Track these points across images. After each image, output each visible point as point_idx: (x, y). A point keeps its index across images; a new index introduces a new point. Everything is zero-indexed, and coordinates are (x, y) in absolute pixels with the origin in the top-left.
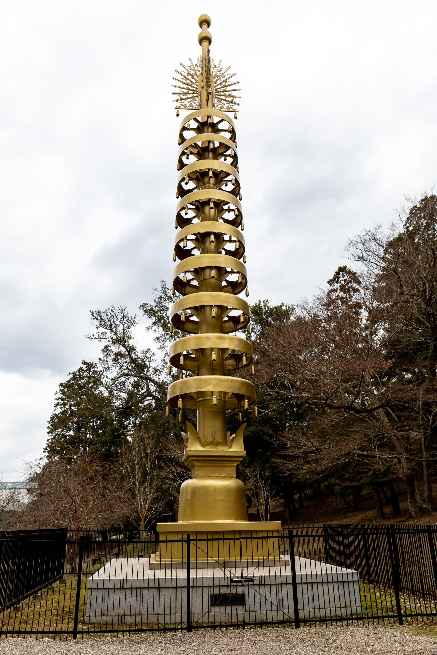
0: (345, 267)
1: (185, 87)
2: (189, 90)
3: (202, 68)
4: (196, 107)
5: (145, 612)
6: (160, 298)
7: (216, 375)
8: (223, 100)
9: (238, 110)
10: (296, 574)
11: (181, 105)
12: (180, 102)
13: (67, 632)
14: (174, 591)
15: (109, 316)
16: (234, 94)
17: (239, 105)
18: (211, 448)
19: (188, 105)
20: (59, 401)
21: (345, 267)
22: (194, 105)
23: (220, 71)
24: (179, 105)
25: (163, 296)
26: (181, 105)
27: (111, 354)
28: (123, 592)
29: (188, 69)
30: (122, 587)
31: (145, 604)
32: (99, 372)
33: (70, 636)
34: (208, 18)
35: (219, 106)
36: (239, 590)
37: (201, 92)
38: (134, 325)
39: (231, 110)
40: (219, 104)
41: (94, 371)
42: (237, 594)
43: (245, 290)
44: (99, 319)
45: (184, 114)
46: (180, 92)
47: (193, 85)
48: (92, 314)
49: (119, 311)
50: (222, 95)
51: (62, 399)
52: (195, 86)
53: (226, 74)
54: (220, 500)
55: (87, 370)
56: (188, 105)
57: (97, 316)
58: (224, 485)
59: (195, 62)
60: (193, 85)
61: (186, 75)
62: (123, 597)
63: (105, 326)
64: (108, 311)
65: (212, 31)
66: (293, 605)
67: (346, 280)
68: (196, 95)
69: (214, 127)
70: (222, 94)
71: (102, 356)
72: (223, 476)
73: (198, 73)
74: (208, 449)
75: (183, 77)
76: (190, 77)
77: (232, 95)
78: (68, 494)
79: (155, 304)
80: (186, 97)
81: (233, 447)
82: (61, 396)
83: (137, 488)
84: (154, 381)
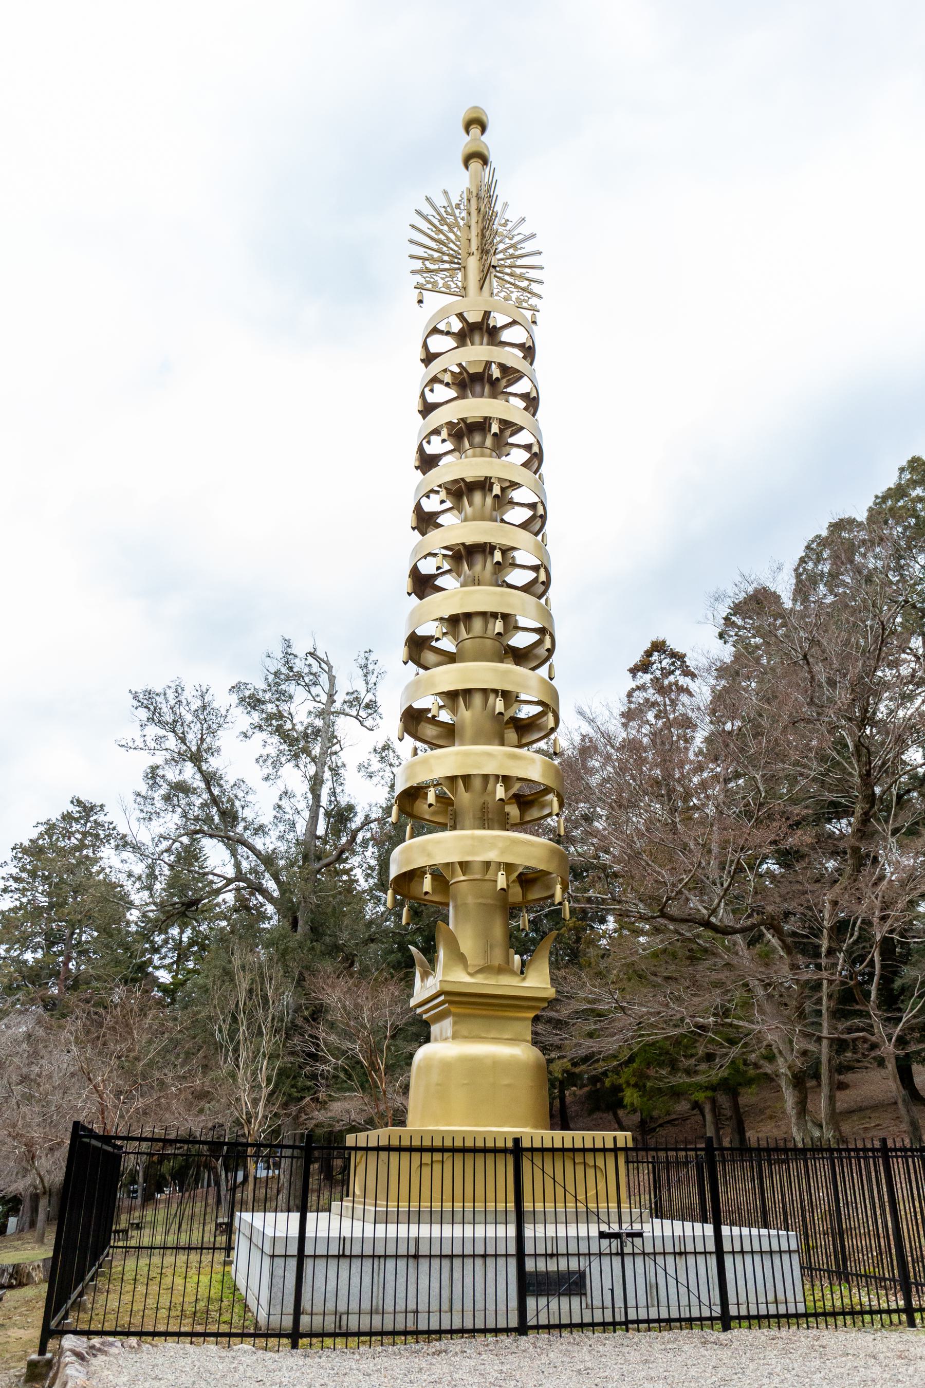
0: (664, 642)
1: (436, 247)
2: (443, 253)
3: (469, 214)
5: (389, 1307)
6: (277, 674)
7: (493, 829)
8: (510, 283)
9: (539, 307)
11: (428, 282)
12: (425, 275)
14: (446, 1263)
15: (172, 702)
16: (532, 274)
17: (540, 297)
18: (486, 979)
19: (441, 285)
20: (8, 884)
21: (664, 642)
22: (453, 286)
23: (505, 225)
24: (422, 281)
25: (284, 670)
26: (428, 282)
27: (161, 783)
28: (344, 1263)
29: (442, 210)
30: (341, 1253)
32: (106, 825)
34: (484, 118)
35: (503, 294)
38: (225, 726)
39: (525, 305)
40: (502, 291)
41: (95, 821)
42: (570, 1273)
43: (548, 664)
44: (152, 708)
46: (426, 255)
47: (452, 245)
48: (135, 697)
49: (195, 693)
50: (507, 274)
51: (17, 879)
52: (456, 248)
53: (515, 233)
54: (506, 1085)
55: (81, 818)
56: (441, 285)
57: (147, 701)
58: (512, 1056)
59: (455, 201)
60: (452, 245)
61: (437, 224)
62: (344, 1274)
63: (162, 723)
64: (168, 691)
65: (491, 141)
67: (665, 668)
68: (456, 266)
69: (492, 334)
70: (508, 270)
71: (143, 789)
72: (506, 1037)
73: (462, 223)
74: (480, 979)
76: (445, 228)
77: (527, 275)
78: (89, 1079)
79: (264, 686)
80: (436, 267)
81: (528, 980)
82: (15, 871)
83: (242, 1072)
84: (255, 849)
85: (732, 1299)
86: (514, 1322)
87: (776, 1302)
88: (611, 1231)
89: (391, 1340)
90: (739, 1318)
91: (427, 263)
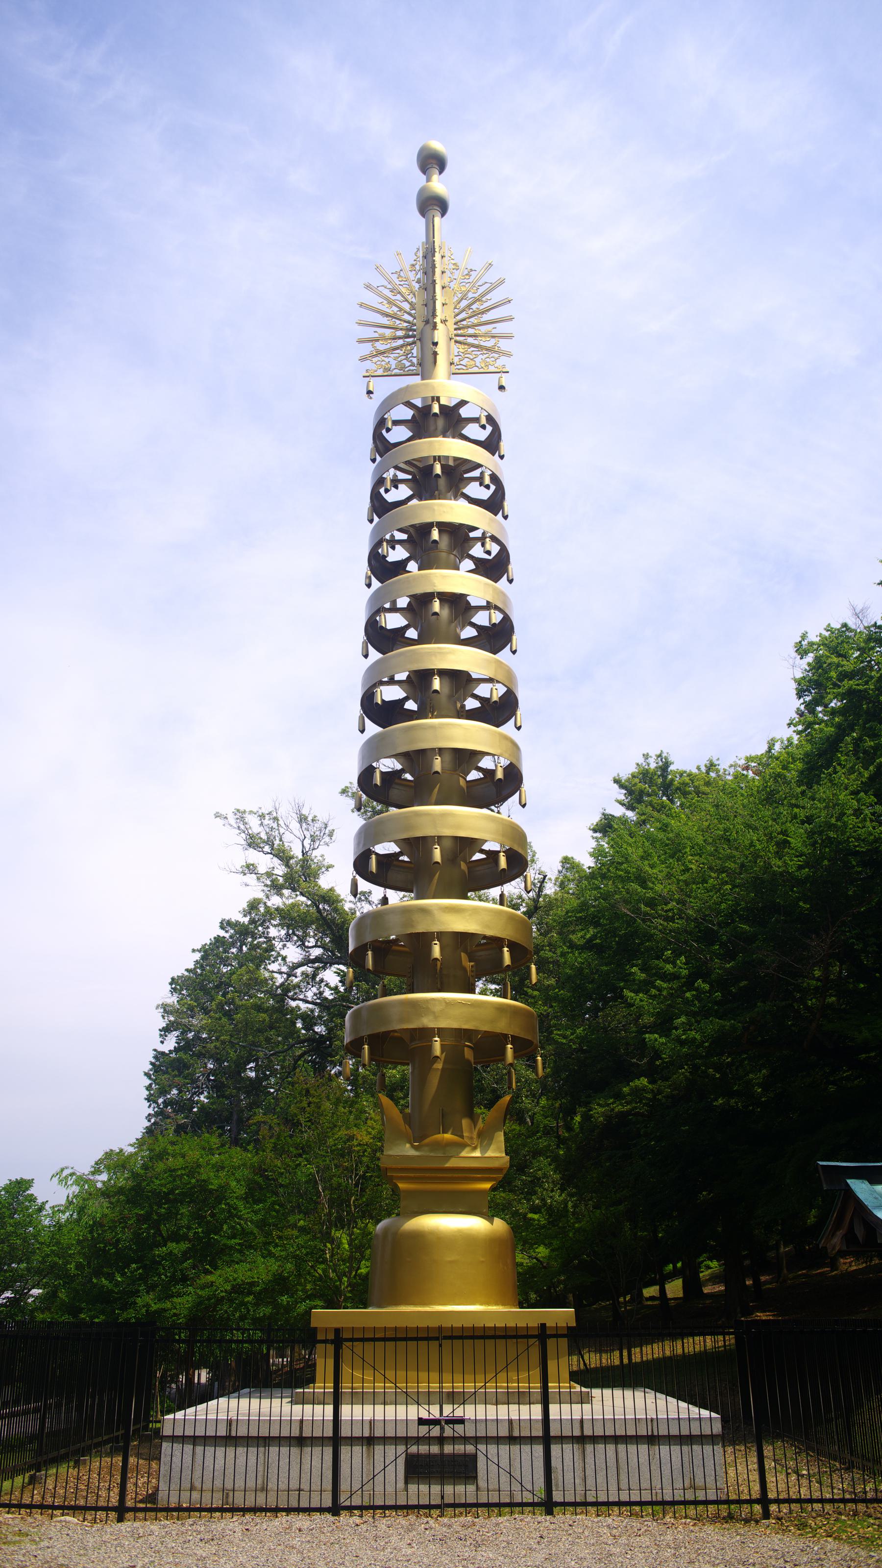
4: (412, 368)
10: (551, 1417)
13: (106, 1509)
16: (500, 328)
31: (273, 1471)
33: (113, 1515)
36: (470, 1449)
37: (422, 333)
42: (465, 1455)
45: (385, 388)
52: (411, 319)
66: (542, 1480)
68: (411, 340)
75: (381, 300)
77: (494, 331)
85: (344, 1486)
86: (328, 1502)
87: (192, 1488)
88: (432, 1417)
89: (133, 1516)
90: (564, 1504)
91: (377, 344)
